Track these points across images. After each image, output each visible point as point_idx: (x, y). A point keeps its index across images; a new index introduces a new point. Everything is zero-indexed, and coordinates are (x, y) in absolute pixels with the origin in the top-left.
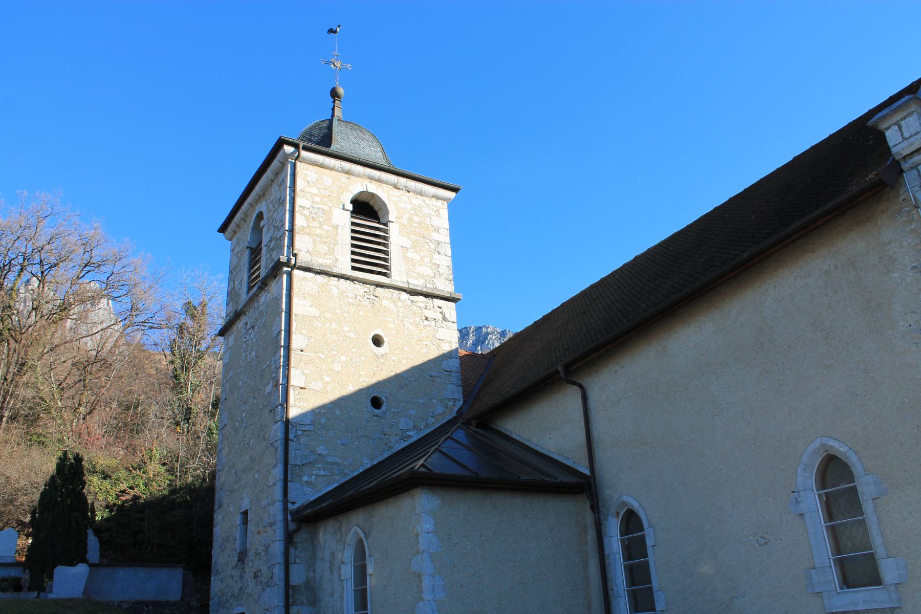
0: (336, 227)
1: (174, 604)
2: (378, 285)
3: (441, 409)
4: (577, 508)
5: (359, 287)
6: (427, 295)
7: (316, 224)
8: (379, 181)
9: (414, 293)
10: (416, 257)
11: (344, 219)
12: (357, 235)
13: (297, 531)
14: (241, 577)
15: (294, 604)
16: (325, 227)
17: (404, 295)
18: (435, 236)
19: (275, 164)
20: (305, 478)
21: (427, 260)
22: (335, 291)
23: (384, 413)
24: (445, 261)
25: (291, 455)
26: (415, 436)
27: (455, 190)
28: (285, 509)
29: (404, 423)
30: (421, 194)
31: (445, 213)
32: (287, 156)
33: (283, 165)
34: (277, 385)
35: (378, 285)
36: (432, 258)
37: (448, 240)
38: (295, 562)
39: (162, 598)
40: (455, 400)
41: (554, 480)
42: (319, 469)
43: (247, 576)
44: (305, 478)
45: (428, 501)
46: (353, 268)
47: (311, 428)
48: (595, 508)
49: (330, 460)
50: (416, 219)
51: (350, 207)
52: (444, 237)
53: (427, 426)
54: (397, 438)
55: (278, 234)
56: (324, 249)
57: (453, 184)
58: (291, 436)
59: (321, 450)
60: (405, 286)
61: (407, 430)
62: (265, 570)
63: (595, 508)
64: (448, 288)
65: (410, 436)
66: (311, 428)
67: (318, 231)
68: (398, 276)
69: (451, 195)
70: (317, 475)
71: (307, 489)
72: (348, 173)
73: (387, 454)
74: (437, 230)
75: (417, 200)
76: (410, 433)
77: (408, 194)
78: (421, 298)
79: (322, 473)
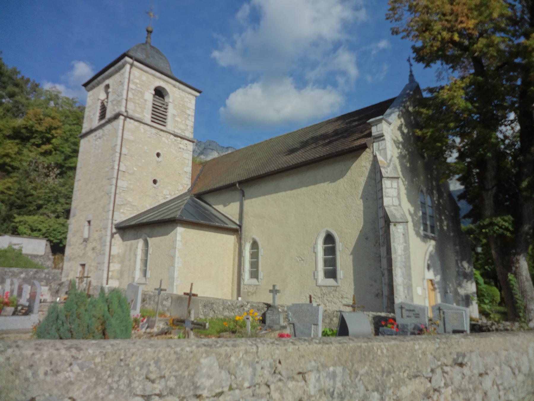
0: (146, 100)
1: (41, 256)
2: (162, 130)
3: (181, 188)
4: (231, 239)
5: (154, 131)
6: (181, 138)
7: (137, 98)
8: (168, 82)
9: (176, 136)
10: (179, 120)
11: (149, 95)
12: (155, 107)
13: (115, 233)
14: (85, 249)
15: (112, 262)
16: (141, 100)
17: (172, 137)
18: (188, 112)
19: (120, 64)
20: (122, 211)
21: (184, 122)
22: (142, 131)
23: (158, 187)
24: (191, 122)
25: (117, 200)
26: (169, 198)
27: (199, 92)
28: (112, 223)
29: (165, 192)
30: (183, 91)
31: (194, 102)
32: (126, 62)
33: (123, 66)
34: (113, 168)
35: (162, 130)
36: (186, 122)
37: (193, 114)
38: (114, 245)
39: (35, 253)
40: (188, 185)
41: (225, 225)
42: (128, 207)
43: (87, 249)
44: (122, 211)
45: (382, 292)
46: (152, 121)
47: (126, 189)
48: (240, 239)
49: (133, 204)
50: (182, 103)
51: (153, 92)
52: (191, 112)
53: (175, 194)
54: (162, 198)
55: (119, 99)
56: (139, 110)
57: (200, 89)
58: (117, 192)
59: (130, 199)
60: (173, 133)
61: (167, 195)
62: (99, 247)
63: (240, 239)
64: (189, 134)
65: (167, 198)
66: (126, 189)
67: (137, 101)
68: (170, 126)
69: (198, 94)
70: (127, 210)
71: (122, 215)
72: (153, 75)
73: (157, 204)
74: (189, 109)
75: (183, 94)
76: (167, 196)
77: (179, 91)
78: (179, 139)
79: (129, 209)
